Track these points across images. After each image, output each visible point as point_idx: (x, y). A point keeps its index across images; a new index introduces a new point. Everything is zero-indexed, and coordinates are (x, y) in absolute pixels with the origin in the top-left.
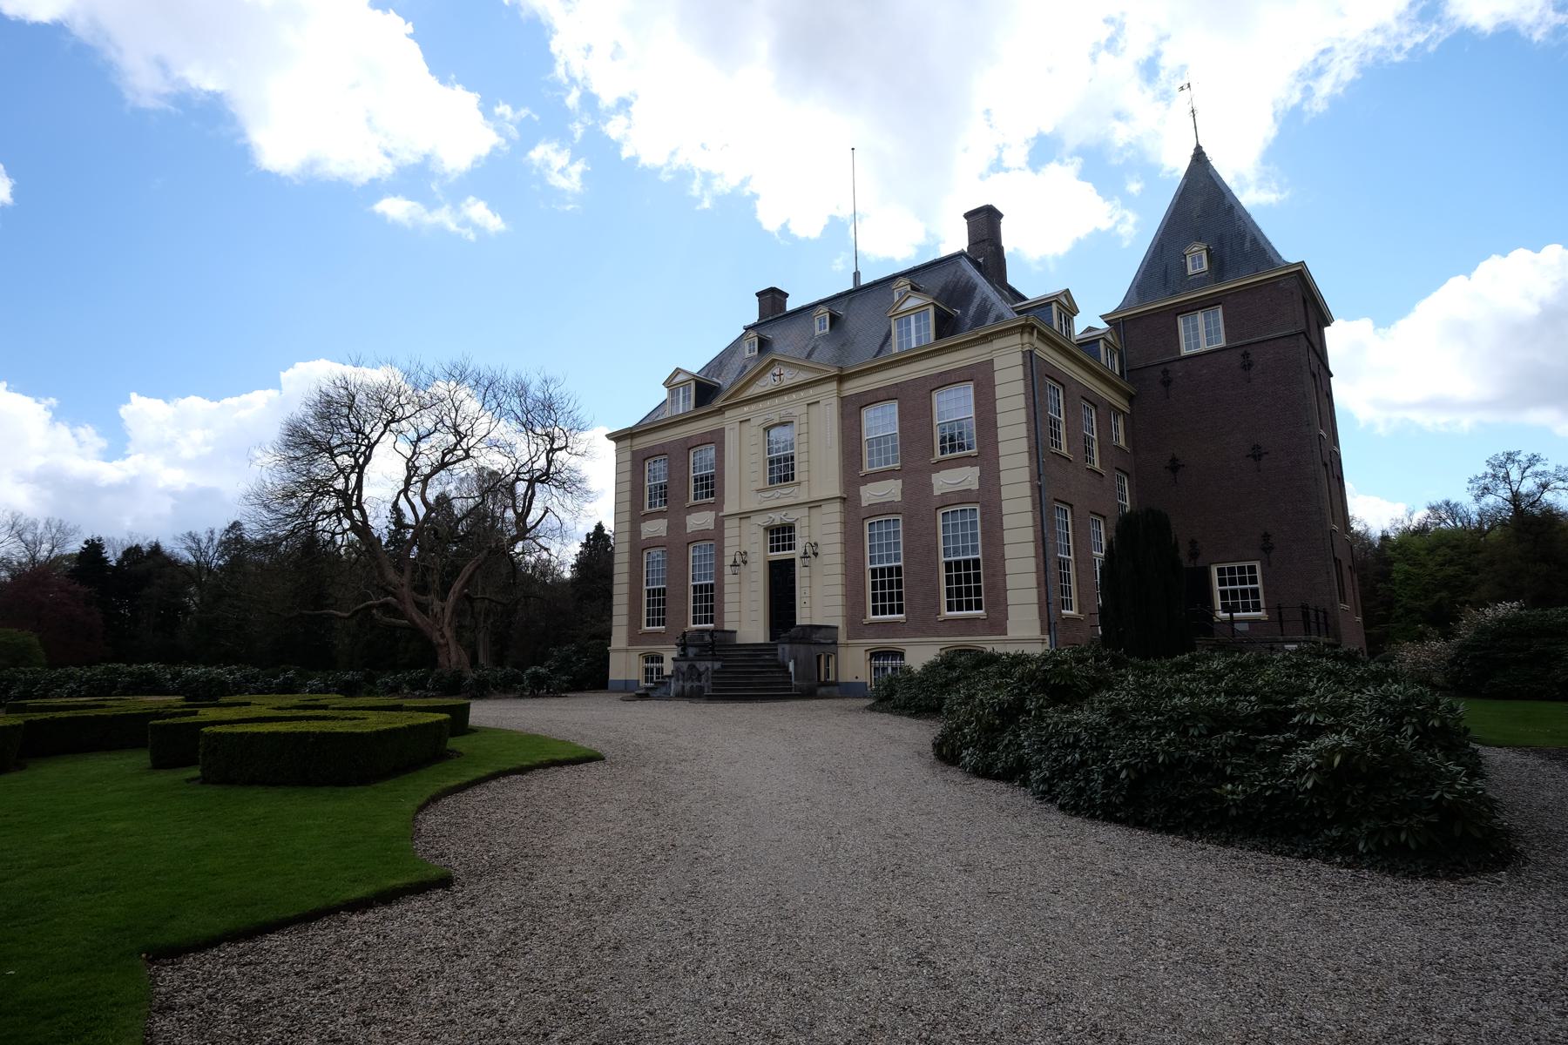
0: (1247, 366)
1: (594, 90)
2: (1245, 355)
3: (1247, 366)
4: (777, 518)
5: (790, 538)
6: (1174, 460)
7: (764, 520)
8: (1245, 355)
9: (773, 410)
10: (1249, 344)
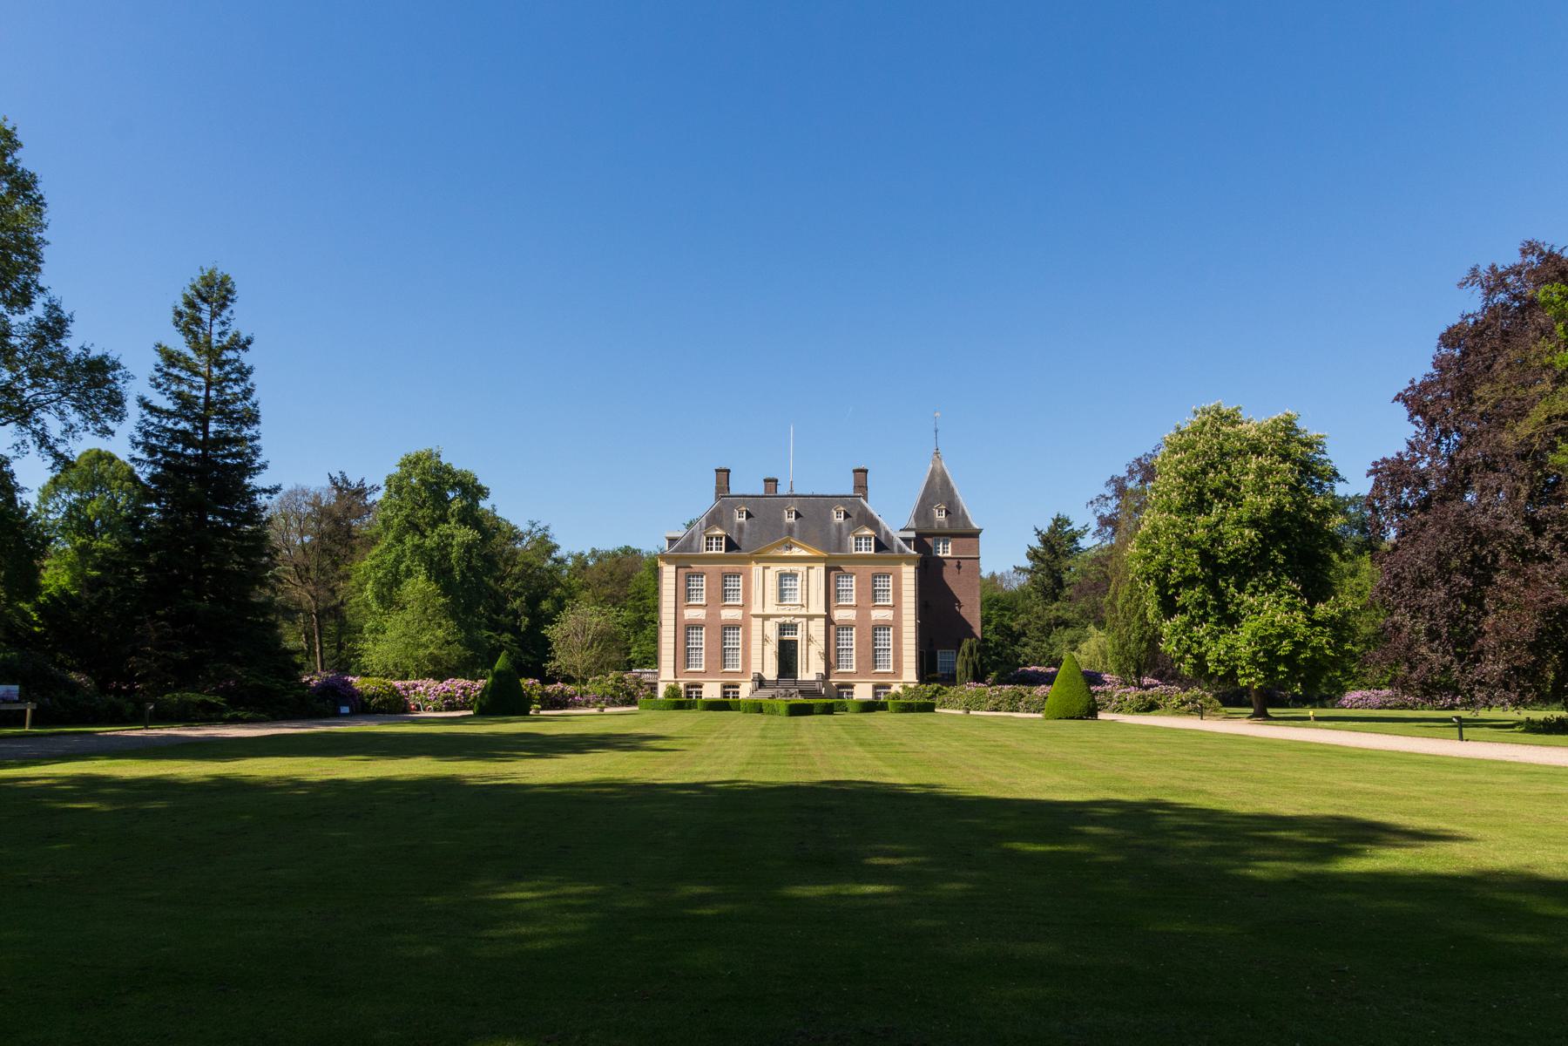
0: (959, 567)
1: (184, 337)
2: (959, 563)
4: (788, 620)
5: (796, 630)
7: (781, 620)
8: (959, 563)
9: (787, 568)
10: (960, 558)
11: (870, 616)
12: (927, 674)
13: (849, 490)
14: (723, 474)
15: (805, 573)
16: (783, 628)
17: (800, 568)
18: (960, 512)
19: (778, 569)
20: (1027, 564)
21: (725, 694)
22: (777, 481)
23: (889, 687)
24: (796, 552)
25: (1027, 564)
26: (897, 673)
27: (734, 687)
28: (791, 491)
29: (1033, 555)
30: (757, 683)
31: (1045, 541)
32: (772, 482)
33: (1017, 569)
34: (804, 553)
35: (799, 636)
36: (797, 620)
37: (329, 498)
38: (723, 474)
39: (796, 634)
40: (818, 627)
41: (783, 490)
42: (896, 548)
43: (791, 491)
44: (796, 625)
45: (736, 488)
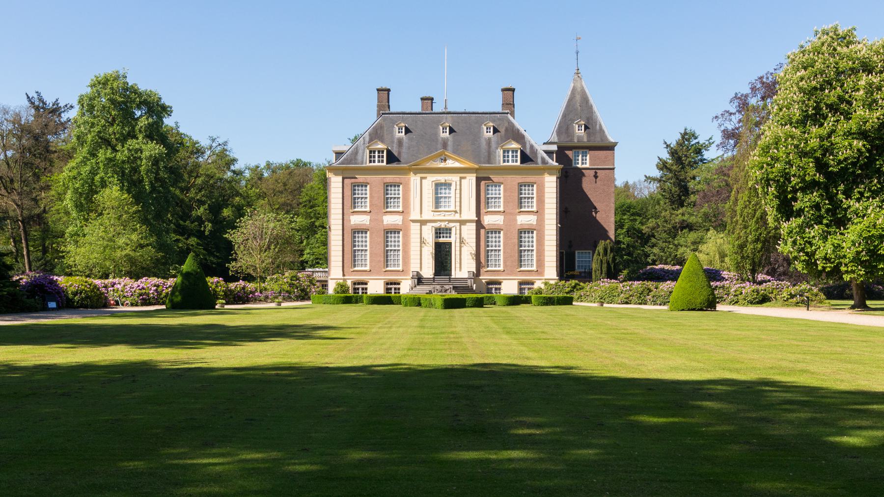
2: (596, 173)
3: (596, 177)
4: (443, 225)
6: (566, 208)
7: (437, 225)
8: (596, 173)
9: (442, 178)
11: (516, 220)
12: (567, 272)
13: (497, 106)
14: (384, 93)
15: (458, 183)
16: (439, 232)
17: (454, 178)
18: (598, 126)
19: (434, 179)
20: (657, 174)
21: (388, 290)
22: (432, 99)
23: (533, 284)
24: (450, 164)
25: (657, 174)
26: (540, 271)
27: (395, 284)
28: (446, 108)
29: (663, 166)
30: (416, 280)
31: (673, 153)
32: (428, 100)
33: (649, 179)
34: (457, 165)
35: (453, 239)
36: (451, 225)
37: (28, 116)
38: (384, 93)
39: (450, 237)
40: (469, 232)
41: (438, 107)
42: (539, 160)
43: (446, 108)
44: (450, 229)
45: (396, 106)
